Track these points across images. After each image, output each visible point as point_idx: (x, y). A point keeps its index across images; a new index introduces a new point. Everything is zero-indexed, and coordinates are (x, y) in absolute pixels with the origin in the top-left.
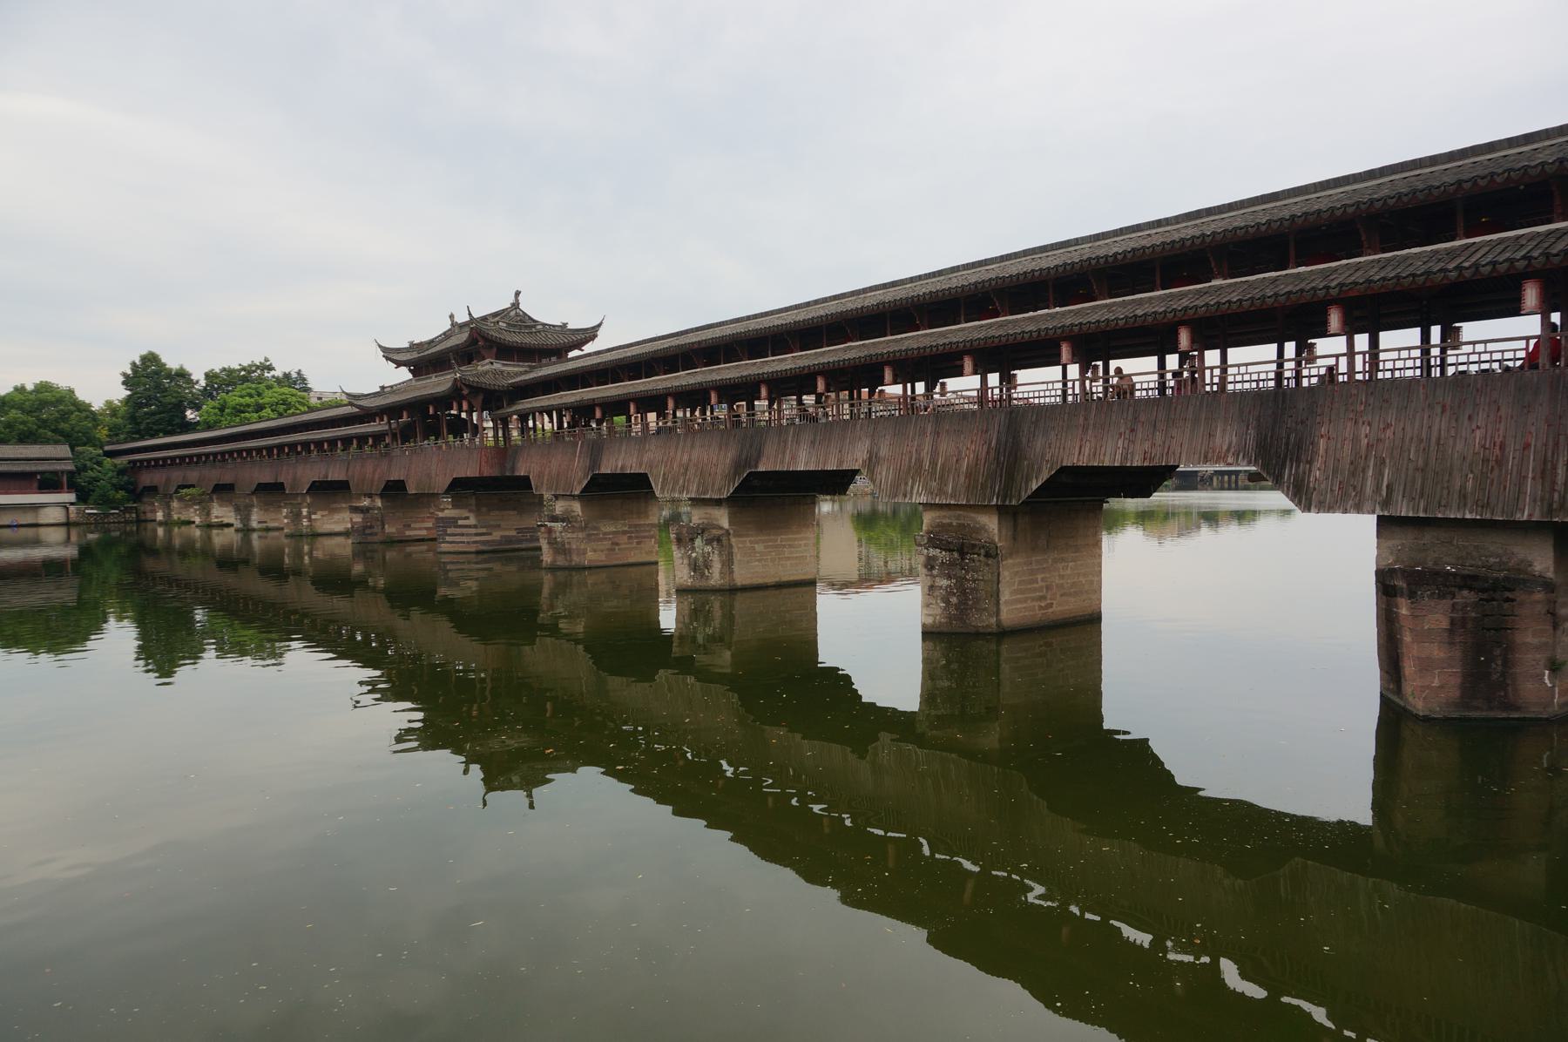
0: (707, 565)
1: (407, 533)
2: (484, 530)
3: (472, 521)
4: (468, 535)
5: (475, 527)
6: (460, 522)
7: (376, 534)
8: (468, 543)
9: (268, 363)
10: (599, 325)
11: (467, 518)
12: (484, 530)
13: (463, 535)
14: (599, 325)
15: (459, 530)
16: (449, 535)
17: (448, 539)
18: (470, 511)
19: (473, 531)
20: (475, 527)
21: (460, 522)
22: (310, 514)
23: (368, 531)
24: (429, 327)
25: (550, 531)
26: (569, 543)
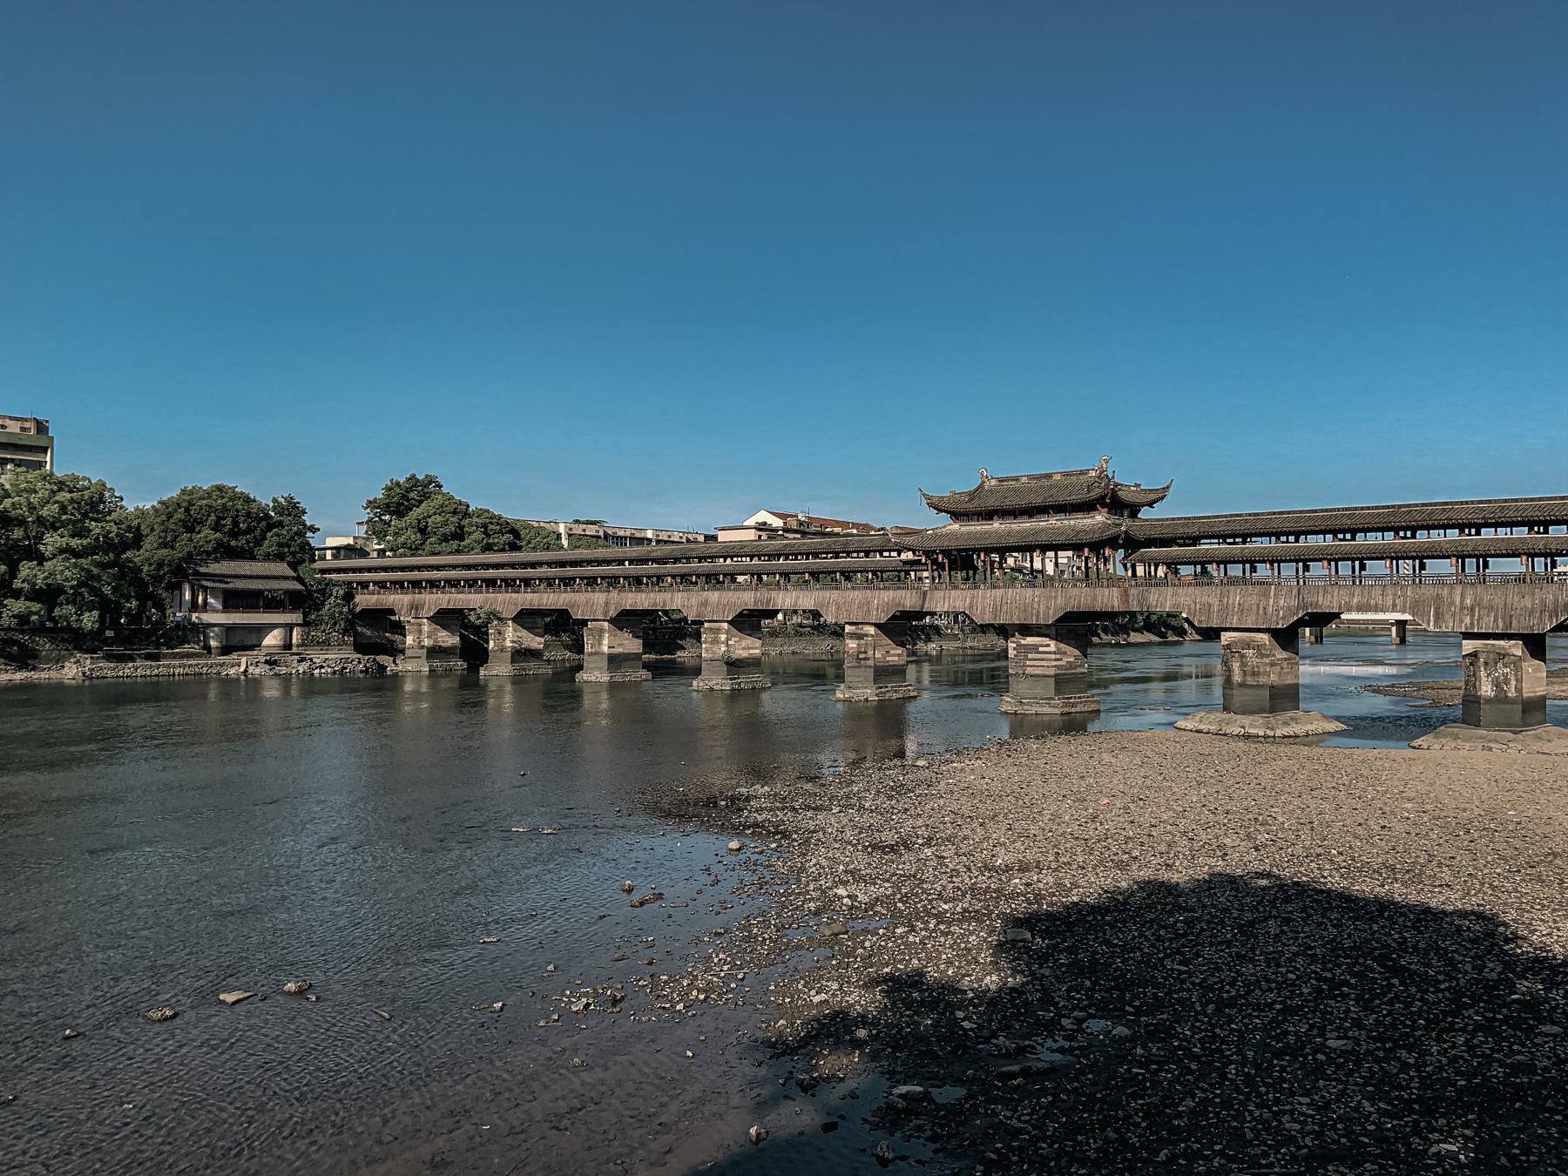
0: (1507, 681)
1: (888, 659)
2: (1058, 656)
3: (1053, 648)
4: (1050, 660)
5: (1054, 653)
6: (1041, 649)
7: (869, 659)
8: (1048, 667)
9: (810, 1092)
10: (1168, 487)
11: (1048, 645)
12: (1058, 656)
13: (1043, 660)
14: (1168, 487)
15: (1039, 656)
16: (1030, 660)
17: (1028, 663)
18: (1051, 638)
19: (1053, 656)
20: (1054, 653)
21: (1041, 649)
22: (728, 639)
23: (862, 656)
24: (761, 521)
25: (1243, 656)
26: (1258, 667)
